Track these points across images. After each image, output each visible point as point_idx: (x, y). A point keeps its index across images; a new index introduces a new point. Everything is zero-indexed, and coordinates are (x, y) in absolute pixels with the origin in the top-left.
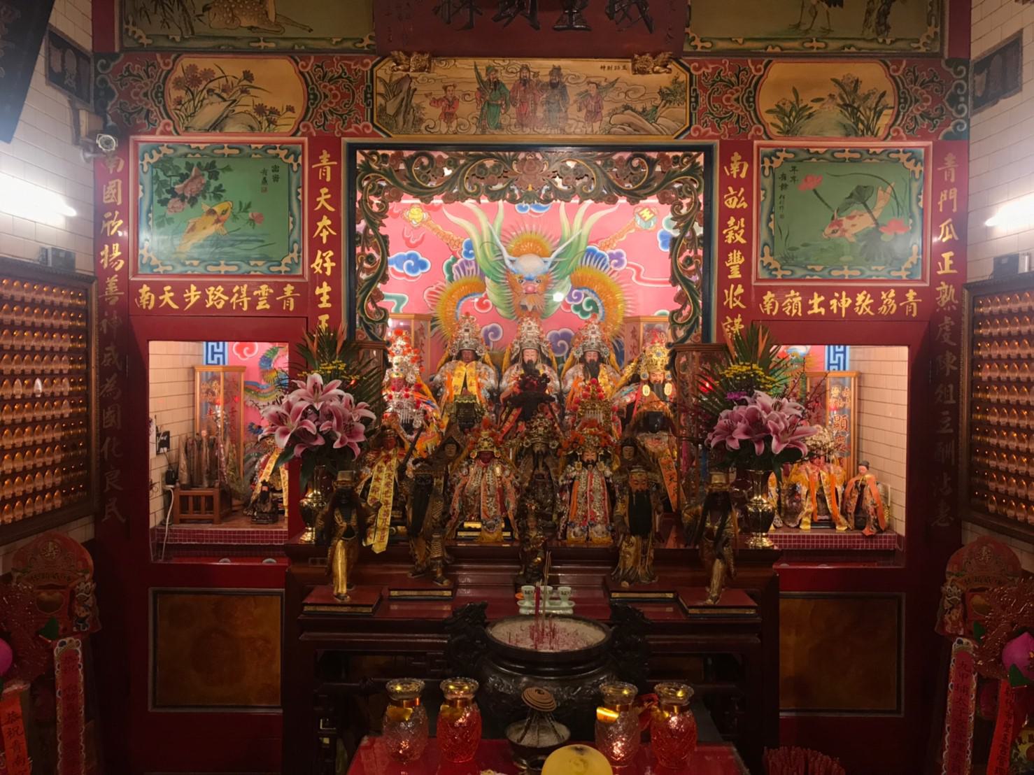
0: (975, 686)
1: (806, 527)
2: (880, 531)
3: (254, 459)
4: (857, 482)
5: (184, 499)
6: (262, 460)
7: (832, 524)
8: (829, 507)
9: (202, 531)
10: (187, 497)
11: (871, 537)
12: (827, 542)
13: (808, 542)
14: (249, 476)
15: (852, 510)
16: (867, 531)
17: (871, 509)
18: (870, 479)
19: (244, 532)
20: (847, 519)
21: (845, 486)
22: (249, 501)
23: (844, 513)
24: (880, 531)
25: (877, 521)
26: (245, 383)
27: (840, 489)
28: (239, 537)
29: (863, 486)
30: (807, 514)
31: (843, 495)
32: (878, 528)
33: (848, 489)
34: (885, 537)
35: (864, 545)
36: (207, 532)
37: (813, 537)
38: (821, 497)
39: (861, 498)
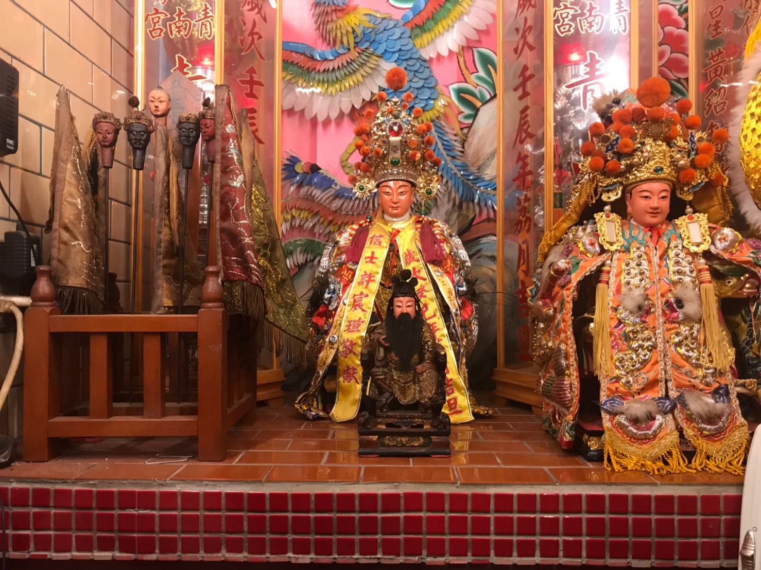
0: (517, 453)
3: (300, 258)
5: (67, 350)
6: (344, 239)
9: (147, 499)
10: (83, 339)
14: (303, 288)
19: (346, 501)
22: (312, 368)
26: (285, 43)
28: (323, 526)
36: (169, 499)
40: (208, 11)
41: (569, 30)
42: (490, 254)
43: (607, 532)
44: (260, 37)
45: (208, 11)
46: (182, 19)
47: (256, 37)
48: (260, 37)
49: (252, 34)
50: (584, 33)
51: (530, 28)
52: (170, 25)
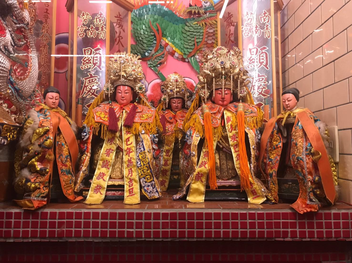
1: (197, 199)
2: (326, 204)
4: (279, 121)
7: (240, 193)
8: (236, 164)
11: (309, 215)
12: (217, 226)
13: (200, 226)
15: (273, 171)
16: (300, 206)
17: (307, 163)
18: (302, 114)
20: (265, 183)
21: (261, 131)
23: (261, 174)
24: (326, 204)
25: (318, 185)
27: (252, 135)
29: (289, 126)
30: (199, 177)
31: (259, 145)
32: (322, 198)
33: (266, 136)
34: (337, 216)
35: (294, 232)
37: (208, 215)
38: (223, 150)
39: (287, 147)
40: (103, 28)
41: (83, 36)
42: (318, 130)
43: (195, 227)
44: (122, 38)
45: (103, 28)
46: (93, 30)
47: (121, 38)
48: (122, 38)
49: (119, 37)
50: (89, 37)
51: (232, 34)
52: (88, 32)
